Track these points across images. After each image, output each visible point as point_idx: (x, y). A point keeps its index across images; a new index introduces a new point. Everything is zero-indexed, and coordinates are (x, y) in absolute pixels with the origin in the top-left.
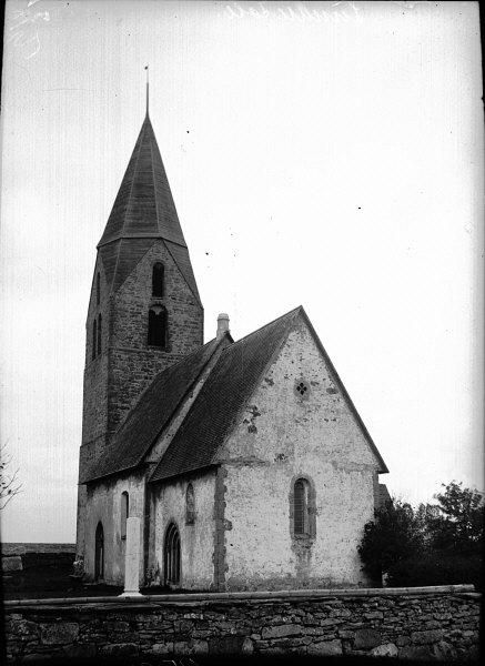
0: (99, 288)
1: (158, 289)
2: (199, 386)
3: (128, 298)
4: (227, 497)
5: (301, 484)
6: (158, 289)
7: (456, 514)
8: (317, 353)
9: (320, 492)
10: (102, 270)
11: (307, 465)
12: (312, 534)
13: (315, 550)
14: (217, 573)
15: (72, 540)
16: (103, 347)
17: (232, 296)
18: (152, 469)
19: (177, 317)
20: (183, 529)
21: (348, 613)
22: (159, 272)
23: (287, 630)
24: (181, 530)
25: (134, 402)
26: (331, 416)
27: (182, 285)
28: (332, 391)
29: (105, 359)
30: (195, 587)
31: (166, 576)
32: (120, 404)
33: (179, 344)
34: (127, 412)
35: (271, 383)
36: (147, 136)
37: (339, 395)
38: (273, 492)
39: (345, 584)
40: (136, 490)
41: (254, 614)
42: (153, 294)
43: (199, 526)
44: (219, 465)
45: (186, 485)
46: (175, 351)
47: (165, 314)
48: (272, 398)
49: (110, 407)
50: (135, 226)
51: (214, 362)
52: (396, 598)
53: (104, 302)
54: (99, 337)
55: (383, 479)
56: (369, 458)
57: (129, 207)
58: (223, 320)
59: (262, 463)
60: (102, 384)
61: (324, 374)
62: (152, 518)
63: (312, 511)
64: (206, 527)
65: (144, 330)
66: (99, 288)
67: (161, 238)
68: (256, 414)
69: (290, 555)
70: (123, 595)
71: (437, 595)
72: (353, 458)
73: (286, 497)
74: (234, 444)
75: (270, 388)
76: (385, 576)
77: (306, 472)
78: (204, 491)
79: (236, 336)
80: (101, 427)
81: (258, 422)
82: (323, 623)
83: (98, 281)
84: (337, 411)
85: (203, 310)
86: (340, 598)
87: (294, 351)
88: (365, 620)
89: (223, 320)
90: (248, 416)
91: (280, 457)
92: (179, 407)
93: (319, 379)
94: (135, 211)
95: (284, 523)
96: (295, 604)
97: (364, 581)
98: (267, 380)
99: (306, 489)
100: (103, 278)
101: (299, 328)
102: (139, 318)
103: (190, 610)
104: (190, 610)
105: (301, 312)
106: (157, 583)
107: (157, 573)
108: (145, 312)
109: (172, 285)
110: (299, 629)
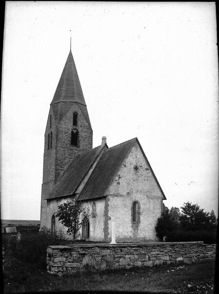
0: (51, 121)
1: (75, 123)
2: (95, 164)
3: (63, 126)
4: (109, 208)
5: (135, 203)
6: (75, 123)
7: (189, 214)
8: (142, 155)
9: (142, 206)
10: (52, 114)
11: (137, 197)
12: (139, 222)
13: (139, 228)
14: (105, 236)
15: (39, 219)
16: (53, 145)
17: (106, 129)
18: (78, 196)
19: (82, 134)
20: (91, 220)
21: (171, 249)
22: (75, 116)
23: (157, 253)
24: (90, 220)
25: (66, 168)
26: (146, 179)
27: (84, 121)
28: (147, 169)
29: (54, 151)
30: (96, 240)
31: (83, 236)
32: (60, 168)
33: (82, 144)
34: (63, 171)
35: (125, 166)
36: (70, 59)
37: (149, 171)
39: (150, 240)
41: (148, 248)
43: (98, 219)
44: (106, 196)
45: (92, 203)
46: (81, 148)
47: (77, 133)
48: (125, 173)
49: (56, 170)
50: (66, 97)
51: (101, 156)
52: (183, 245)
53: (54, 127)
54: (51, 143)
55: (164, 201)
56: (160, 194)
57: (64, 89)
58: (104, 139)
59: (121, 196)
60: (53, 160)
63: (139, 213)
64: (100, 220)
65: (70, 139)
66: (51, 121)
67: (76, 102)
68: (120, 178)
69: (130, 229)
70: (111, 243)
71: (194, 244)
72: (154, 194)
74: (112, 189)
76: (165, 237)
77: (137, 199)
78: (100, 206)
79: (110, 145)
80: (52, 177)
81: (120, 181)
82: (165, 251)
83: (51, 119)
84: (149, 176)
86: (169, 244)
87: (134, 154)
88: (175, 251)
89: (104, 139)
90: (117, 178)
91: (128, 193)
92: (88, 172)
94: (66, 91)
95: (128, 217)
96: (158, 246)
97: (157, 239)
98: (124, 165)
99: (137, 205)
100: (53, 117)
101: (136, 146)
102: (68, 134)
103: (134, 247)
104: (134, 247)
105: (137, 140)
106: (80, 239)
107: (79, 235)
108: (70, 132)
110: (159, 253)
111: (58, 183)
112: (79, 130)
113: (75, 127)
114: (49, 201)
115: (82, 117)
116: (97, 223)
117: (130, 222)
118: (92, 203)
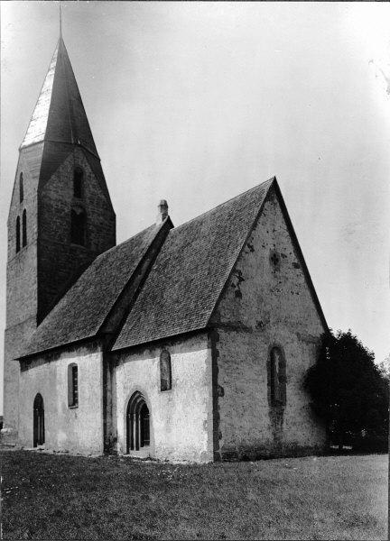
6: (78, 190)
20: (155, 400)
28: (296, 266)
38: (256, 358)
40: (90, 363)
42: (74, 195)
43: (178, 394)
47: (84, 216)
59: (247, 329)
61: (290, 249)
62: (109, 387)
68: (241, 280)
73: (265, 365)
75: (251, 255)
77: (279, 341)
85: (113, 217)
91: (260, 324)
93: (287, 253)
109: (90, 188)
111: (45, 322)
112: (89, 209)
113: (77, 201)
114: (26, 362)
115: (94, 182)
116: (179, 407)
117: (266, 403)
118: (158, 351)
